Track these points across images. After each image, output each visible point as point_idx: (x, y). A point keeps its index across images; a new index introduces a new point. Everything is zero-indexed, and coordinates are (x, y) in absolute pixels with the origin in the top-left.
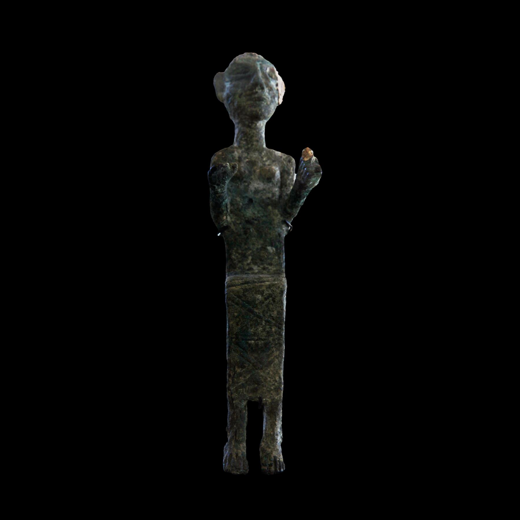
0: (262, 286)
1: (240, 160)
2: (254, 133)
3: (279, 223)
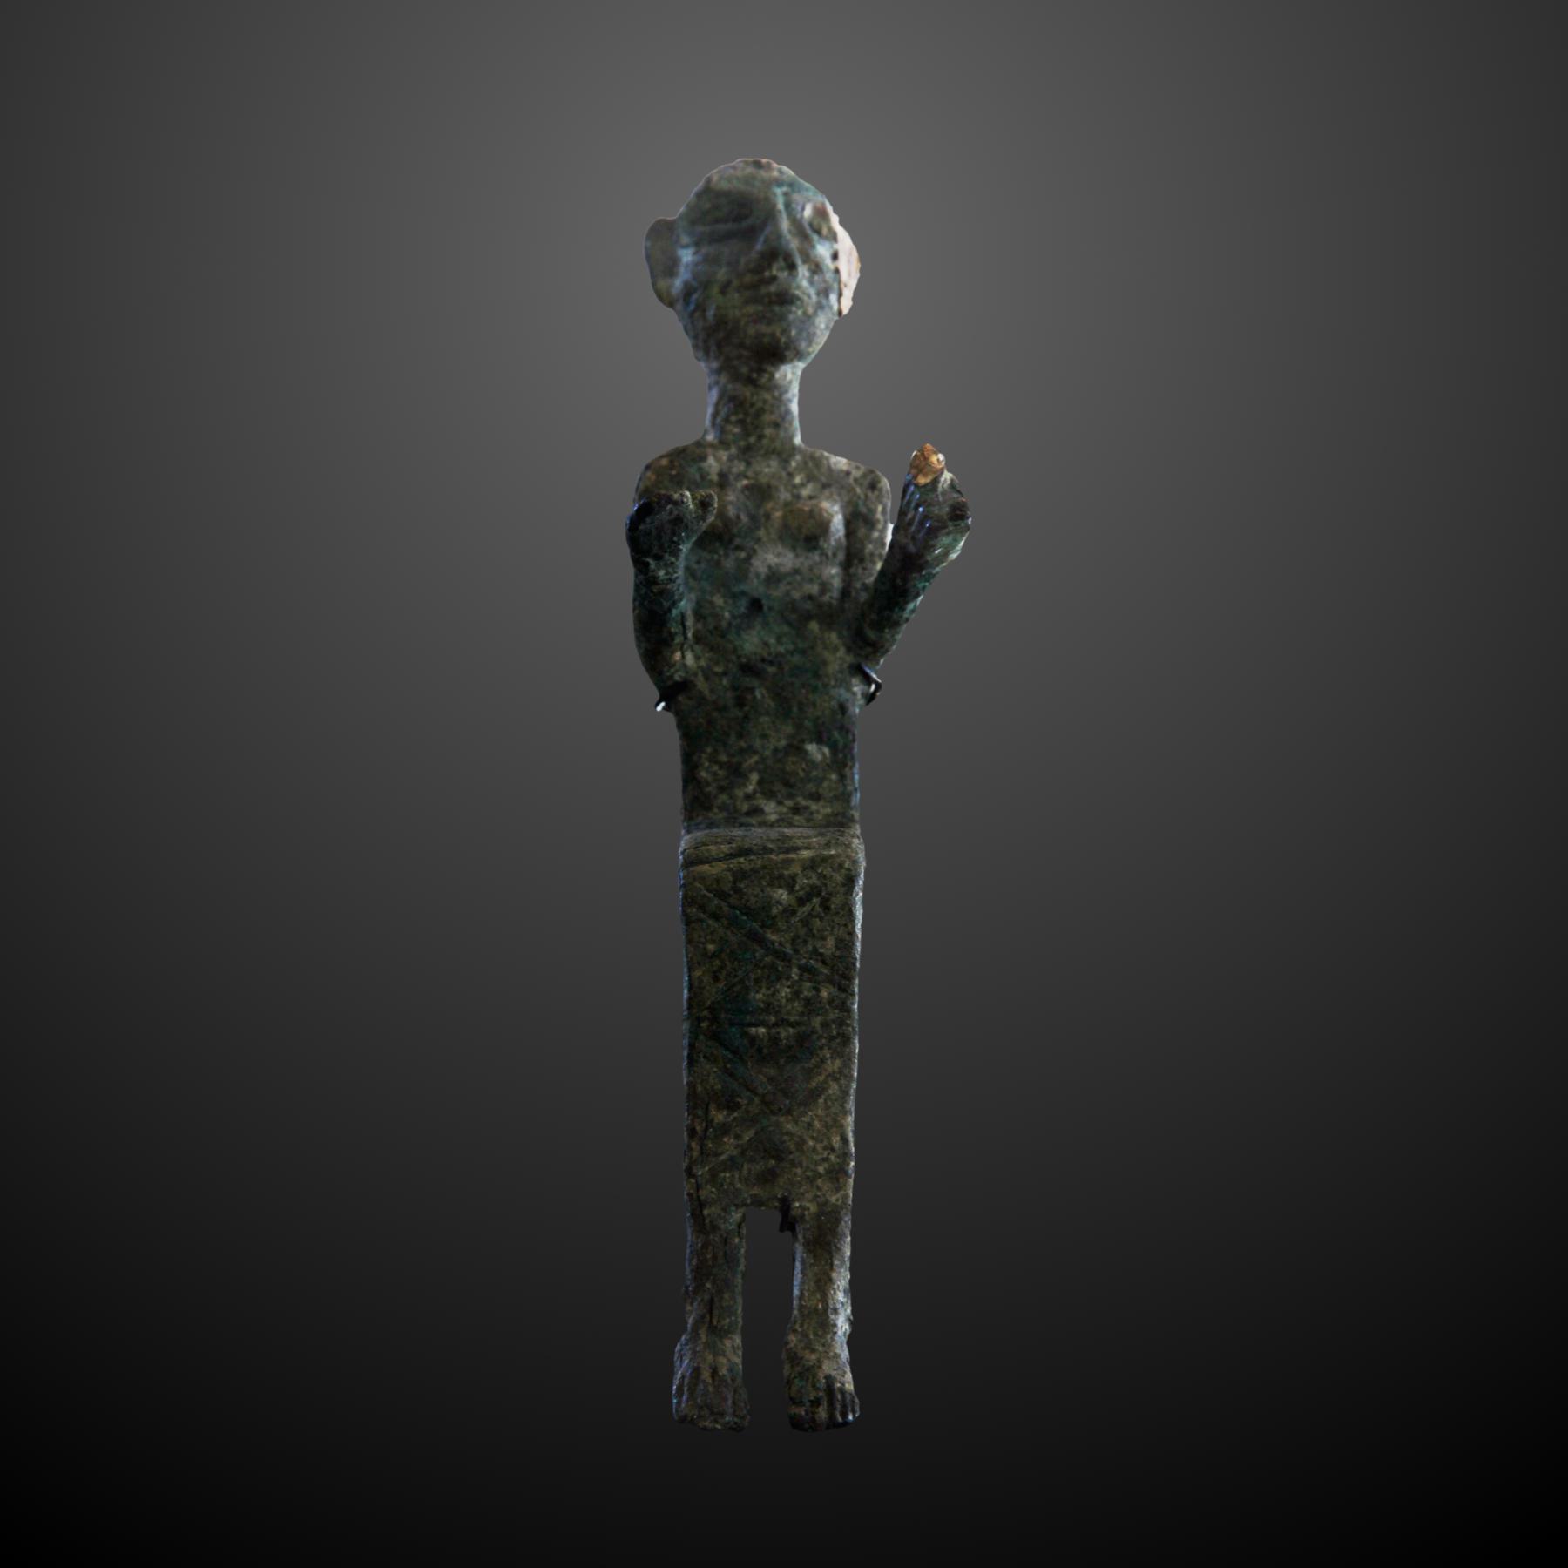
0: (789, 862)
1: (723, 482)
2: (765, 401)
3: (841, 672)
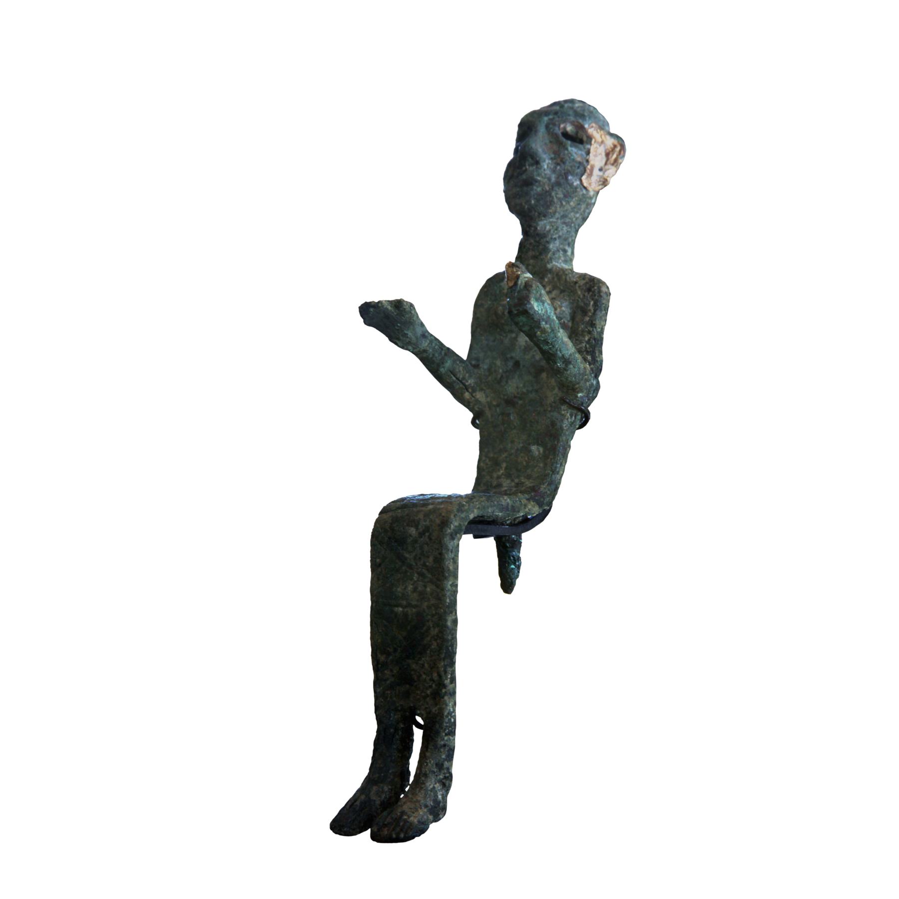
0: (419, 512)
2: (531, 244)
3: (555, 402)
